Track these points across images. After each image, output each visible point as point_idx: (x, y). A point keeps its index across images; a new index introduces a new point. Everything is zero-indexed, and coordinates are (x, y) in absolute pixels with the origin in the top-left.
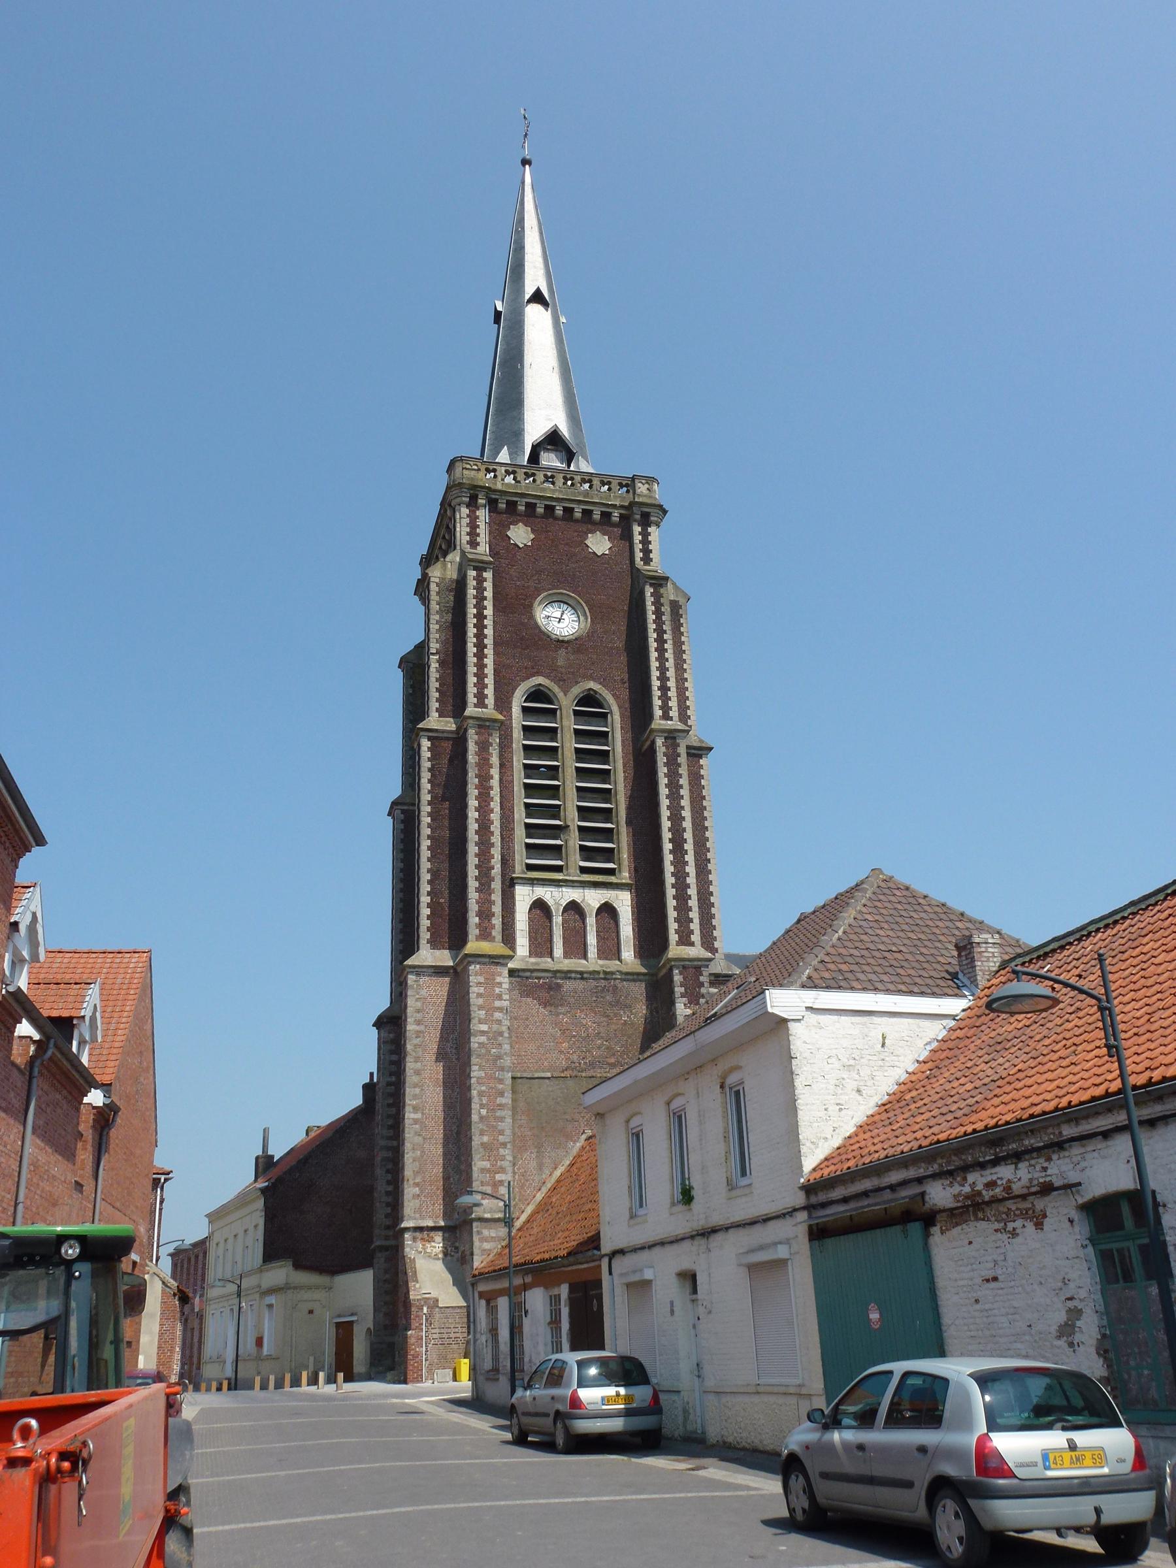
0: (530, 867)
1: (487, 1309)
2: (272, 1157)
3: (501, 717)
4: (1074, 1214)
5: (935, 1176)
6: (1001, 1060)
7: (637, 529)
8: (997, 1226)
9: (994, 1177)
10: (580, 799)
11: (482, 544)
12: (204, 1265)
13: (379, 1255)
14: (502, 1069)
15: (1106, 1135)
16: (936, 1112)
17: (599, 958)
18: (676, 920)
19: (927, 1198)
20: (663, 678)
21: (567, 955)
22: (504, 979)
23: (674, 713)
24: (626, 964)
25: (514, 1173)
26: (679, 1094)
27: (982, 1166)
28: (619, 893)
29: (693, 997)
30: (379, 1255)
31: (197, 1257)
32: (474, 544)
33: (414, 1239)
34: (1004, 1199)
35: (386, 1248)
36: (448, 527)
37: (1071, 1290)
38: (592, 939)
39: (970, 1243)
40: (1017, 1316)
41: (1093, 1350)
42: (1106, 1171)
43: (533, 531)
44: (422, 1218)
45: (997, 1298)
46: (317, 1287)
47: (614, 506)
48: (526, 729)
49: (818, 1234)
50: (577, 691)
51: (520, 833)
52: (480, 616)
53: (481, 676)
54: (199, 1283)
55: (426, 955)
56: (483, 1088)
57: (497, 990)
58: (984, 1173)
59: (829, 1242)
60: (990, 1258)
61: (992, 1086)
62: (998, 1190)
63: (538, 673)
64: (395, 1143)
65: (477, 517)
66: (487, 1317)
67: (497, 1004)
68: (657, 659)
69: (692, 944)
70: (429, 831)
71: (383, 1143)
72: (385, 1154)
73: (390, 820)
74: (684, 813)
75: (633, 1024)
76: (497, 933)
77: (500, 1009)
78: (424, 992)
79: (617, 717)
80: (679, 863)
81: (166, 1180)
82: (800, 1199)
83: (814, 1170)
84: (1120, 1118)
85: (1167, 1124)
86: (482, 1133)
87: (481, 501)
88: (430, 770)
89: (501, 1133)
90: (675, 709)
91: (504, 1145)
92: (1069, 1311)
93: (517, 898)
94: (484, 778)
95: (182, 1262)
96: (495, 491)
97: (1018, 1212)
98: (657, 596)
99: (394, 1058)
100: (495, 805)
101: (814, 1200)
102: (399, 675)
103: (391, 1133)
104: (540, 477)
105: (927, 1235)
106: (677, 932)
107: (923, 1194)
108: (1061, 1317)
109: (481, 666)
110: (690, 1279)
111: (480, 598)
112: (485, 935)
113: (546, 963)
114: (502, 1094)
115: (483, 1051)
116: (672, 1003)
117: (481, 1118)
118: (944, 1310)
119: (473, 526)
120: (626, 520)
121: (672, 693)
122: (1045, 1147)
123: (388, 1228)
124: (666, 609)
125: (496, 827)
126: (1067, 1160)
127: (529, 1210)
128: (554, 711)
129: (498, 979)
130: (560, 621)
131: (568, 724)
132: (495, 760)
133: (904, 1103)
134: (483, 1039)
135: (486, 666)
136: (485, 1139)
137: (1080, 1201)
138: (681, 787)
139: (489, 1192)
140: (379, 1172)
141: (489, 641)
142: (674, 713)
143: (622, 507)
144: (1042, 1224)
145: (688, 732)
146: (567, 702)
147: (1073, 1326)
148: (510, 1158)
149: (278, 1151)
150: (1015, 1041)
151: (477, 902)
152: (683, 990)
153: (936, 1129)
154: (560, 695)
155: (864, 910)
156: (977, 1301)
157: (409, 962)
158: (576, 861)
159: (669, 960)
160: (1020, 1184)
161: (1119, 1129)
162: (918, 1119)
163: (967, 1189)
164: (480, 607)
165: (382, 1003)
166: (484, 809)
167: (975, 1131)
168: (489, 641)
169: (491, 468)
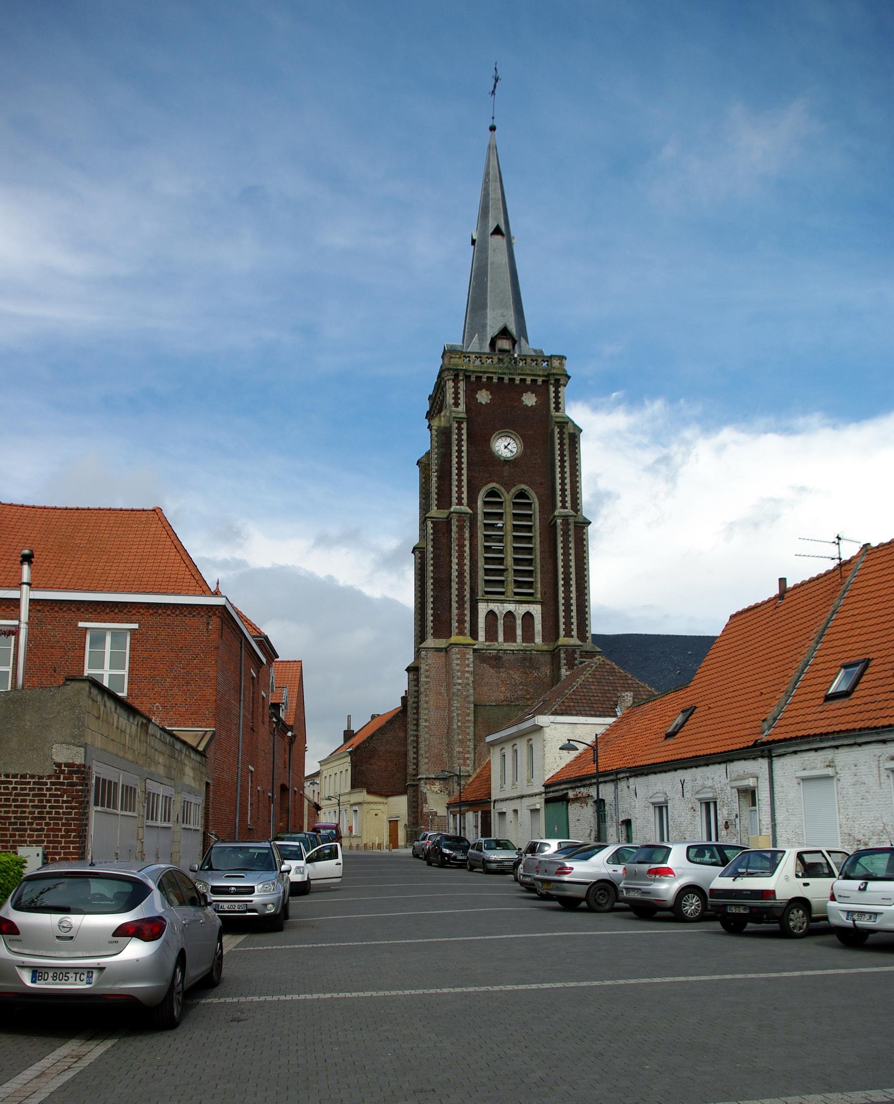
0: (487, 593)
3: (470, 511)
5: (572, 788)
7: (552, 389)
10: (515, 553)
17: (523, 642)
18: (564, 623)
20: (563, 484)
21: (505, 640)
22: (470, 656)
23: (568, 505)
28: (534, 606)
29: (571, 665)
32: (456, 404)
33: (426, 784)
35: (414, 786)
38: (519, 632)
43: (491, 394)
47: (539, 376)
49: (547, 801)
50: (514, 490)
51: (481, 573)
53: (460, 486)
55: (430, 642)
63: (493, 481)
67: (467, 669)
69: (572, 636)
70: (432, 575)
71: (411, 733)
72: (412, 738)
74: (571, 564)
75: (540, 678)
76: (467, 631)
77: (468, 672)
78: (429, 661)
79: (537, 505)
80: (567, 591)
82: (543, 789)
86: (458, 734)
87: (461, 378)
88: (432, 540)
89: (468, 734)
91: (469, 740)
93: (479, 610)
94: (461, 546)
96: (469, 371)
98: (561, 433)
100: (467, 561)
102: (417, 468)
106: (564, 630)
110: (516, 811)
111: (460, 440)
112: (461, 633)
113: (496, 645)
114: (469, 715)
116: (559, 668)
117: (458, 727)
119: (456, 393)
120: (546, 383)
128: (501, 503)
130: (505, 447)
131: (509, 510)
132: (467, 535)
134: (459, 687)
136: (460, 737)
141: (464, 466)
142: (568, 505)
143: (543, 376)
146: (507, 497)
154: (505, 493)
157: (422, 646)
158: (511, 588)
159: (558, 646)
161: (594, 783)
165: (410, 660)
166: (461, 564)
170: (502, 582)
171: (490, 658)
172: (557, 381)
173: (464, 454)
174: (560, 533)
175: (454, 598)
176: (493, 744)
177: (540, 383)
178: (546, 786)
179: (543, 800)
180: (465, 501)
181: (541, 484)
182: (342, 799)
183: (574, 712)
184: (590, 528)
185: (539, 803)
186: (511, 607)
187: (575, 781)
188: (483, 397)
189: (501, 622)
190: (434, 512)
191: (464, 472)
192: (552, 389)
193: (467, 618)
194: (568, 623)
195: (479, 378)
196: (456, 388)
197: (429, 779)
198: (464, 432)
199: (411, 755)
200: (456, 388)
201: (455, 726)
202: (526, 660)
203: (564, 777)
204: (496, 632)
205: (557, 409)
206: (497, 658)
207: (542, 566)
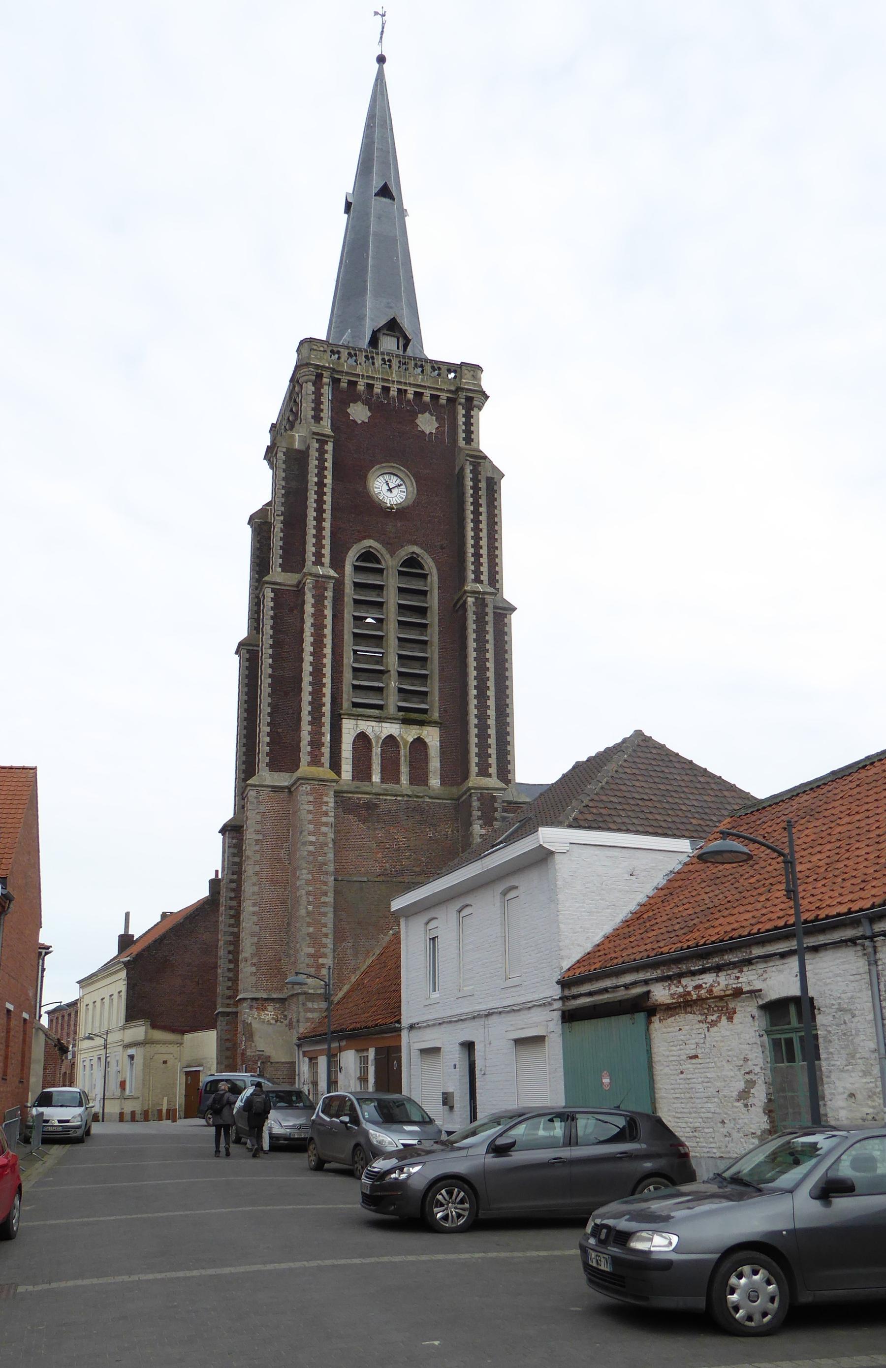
1: (310, 1067)
2: (133, 936)
4: (756, 1012)
5: (658, 980)
6: (717, 892)
7: (461, 411)
8: (700, 1018)
9: (701, 982)
11: (325, 419)
12: (76, 1021)
13: (220, 1018)
14: (327, 873)
15: (783, 955)
16: (664, 930)
17: (411, 783)
18: (477, 755)
19: (651, 994)
20: (477, 546)
21: (383, 780)
22: (330, 800)
23: (484, 577)
24: (434, 790)
25: (334, 958)
26: (467, 906)
27: (693, 974)
29: (488, 820)
30: (220, 1018)
31: (70, 1015)
32: (317, 418)
33: (251, 1008)
34: (707, 999)
35: (228, 1014)
36: (295, 401)
37: (749, 1066)
39: (680, 1030)
40: (709, 1084)
41: (761, 1110)
42: (779, 981)
44: (258, 991)
45: (697, 1071)
46: (170, 1043)
48: (357, 585)
49: (569, 1017)
52: (321, 484)
53: (319, 537)
54: (72, 1036)
55: (265, 776)
56: (311, 889)
57: (324, 808)
58: (693, 978)
59: (578, 1026)
60: (694, 1041)
61: (708, 912)
62: (703, 992)
64: (236, 930)
65: (322, 395)
66: (310, 1071)
67: (324, 819)
68: (472, 529)
69: (490, 776)
70: (270, 671)
73: (237, 658)
77: (326, 824)
79: (435, 578)
80: (482, 706)
81: (46, 954)
82: (556, 991)
83: (569, 969)
84: (793, 944)
85: (826, 949)
87: (325, 380)
90: (486, 574)
91: (326, 935)
92: (747, 1082)
93: (344, 731)
95: (57, 1018)
97: (716, 1009)
99: (237, 859)
101: (567, 993)
102: (248, 531)
103: (232, 921)
104: (378, 362)
105: (649, 1022)
106: (477, 765)
107: (649, 992)
108: (741, 1085)
109: (319, 528)
111: (321, 468)
114: (326, 894)
115: (311, 858)
118: (657, 1078)
119: (318, 402)
121: (484, 560)
122: (738, 962)
123: (229, 997)
124: (483, 485)
125: (328, 670)
126: (754, 972)
127: (346, 988)
129: (325, 799)
130: (390, 490)
131: (392, 582)
133: (642, 920)
134: (311, 848)
135: (324, 529)
136: (311, 930)
137: (761, 1003)
138: (487, 641)
139: (313, 973)
140: (222, 952)
141: (327, 507)
142: (484, 577)
144: (732, 1018)
145: (495, 594)
146: (391, 563)
147: (749, 1092)
148: (331, 946)
149: (137, 931)
150: (731, 877)
151: (310, 733)
152: (479, 813)
153: (661, 944)
154: (388, 557)
155: (625, 764)
156: (682, 1073)
159: (469, 789)
160: (718, 988)
162: (650, 935)
163: (681, 990)
164: (321, 476)
165: (227, 813)
167: (689, 947)
168: (327, 507)
169: (335, 349)
170: (380, 690)
171: (358, 806)
172: (469, 400)
173: (328, 490)
174: (471, 617)
175: (306, 708)
176: (410, 912)
177: (443, 401)
178: (564, 984)
179: (557, 1015)
180: (326, 560)
181: (442, 548)
182: (111, 1038)
183: (612, 826)
184: (514, 617)
185: (545, 1022)
186: (391, 729)
187: (677, 961)
188: (359, 413)
189: (377, 751)
190: (277, 574)
191: (327, 515)
192: (461, 411)
193: (327, 738)
194: (483, 755)
195: (353, 384)
196: (318, 394)
197: (257, 999)
198: (329, 456)
199: (223, 964)
200: (318, 394)
201: (303, 912)
202: (417, 811)
203: (638, 953)
204: (369, 767)
205: (469, 439)
206: (370, 806)
207: (442, 670)
